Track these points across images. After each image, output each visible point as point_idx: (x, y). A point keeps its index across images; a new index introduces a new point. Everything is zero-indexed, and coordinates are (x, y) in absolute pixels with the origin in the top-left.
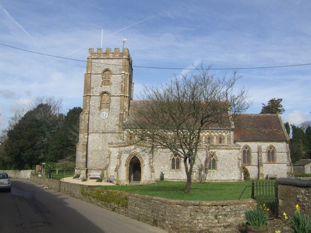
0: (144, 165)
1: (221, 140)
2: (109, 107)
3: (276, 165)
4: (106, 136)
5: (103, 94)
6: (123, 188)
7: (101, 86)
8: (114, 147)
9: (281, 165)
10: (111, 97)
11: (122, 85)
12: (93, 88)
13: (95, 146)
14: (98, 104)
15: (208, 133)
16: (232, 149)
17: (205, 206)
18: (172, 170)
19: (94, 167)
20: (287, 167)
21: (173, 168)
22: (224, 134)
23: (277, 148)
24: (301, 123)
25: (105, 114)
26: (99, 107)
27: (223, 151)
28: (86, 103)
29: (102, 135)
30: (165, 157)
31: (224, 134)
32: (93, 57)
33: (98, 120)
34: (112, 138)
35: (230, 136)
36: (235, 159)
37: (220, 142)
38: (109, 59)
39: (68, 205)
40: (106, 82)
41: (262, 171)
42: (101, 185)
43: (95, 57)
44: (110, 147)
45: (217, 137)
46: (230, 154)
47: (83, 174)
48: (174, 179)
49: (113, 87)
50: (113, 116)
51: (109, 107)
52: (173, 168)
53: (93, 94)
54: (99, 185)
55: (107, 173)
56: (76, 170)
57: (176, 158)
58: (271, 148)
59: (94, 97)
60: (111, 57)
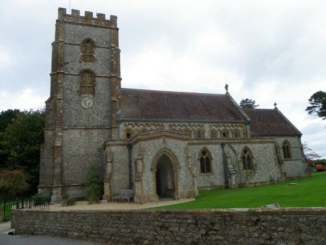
0: (180, 168)
1: (236, 134)
2: (93, 93)
3: (293, 162)
5: (84, 72)
6: (15, 211)
7: (80, 62)
8: (118, 145)
9: (297, 161)
10: (97, 79)
11: (112, 62)
12: (68, 63)
14: (76, 87)
15: (223, 128)
16: (266, 142)
17: (265, 221)
19: (73, 182)
20: (303, 163)
21: (203, 171)
22: (240, 128)
23: (291, 143)
25: (88, 101)
26: (78, 91)
27: (257, 145)
28: (57, 84)
29: (83, 132)
31: (240, 128)
32: (66, 20)
33: (76, 110)
35: (246, 131)
36: (271, 155)
37: (236, 136)
38: (90, 25)
40: (88, 57)
42: (164, 205)
45: (221, 132)
46: (265, 148)
47: (57, 194)
48: (206, 187)
50: (101, 105)
51: (93, 93)
54: (170, 204)
55: (110, 186)
56: (39, 190)
58: (285, 143)
59: (70, 77)
60: (93, 24)
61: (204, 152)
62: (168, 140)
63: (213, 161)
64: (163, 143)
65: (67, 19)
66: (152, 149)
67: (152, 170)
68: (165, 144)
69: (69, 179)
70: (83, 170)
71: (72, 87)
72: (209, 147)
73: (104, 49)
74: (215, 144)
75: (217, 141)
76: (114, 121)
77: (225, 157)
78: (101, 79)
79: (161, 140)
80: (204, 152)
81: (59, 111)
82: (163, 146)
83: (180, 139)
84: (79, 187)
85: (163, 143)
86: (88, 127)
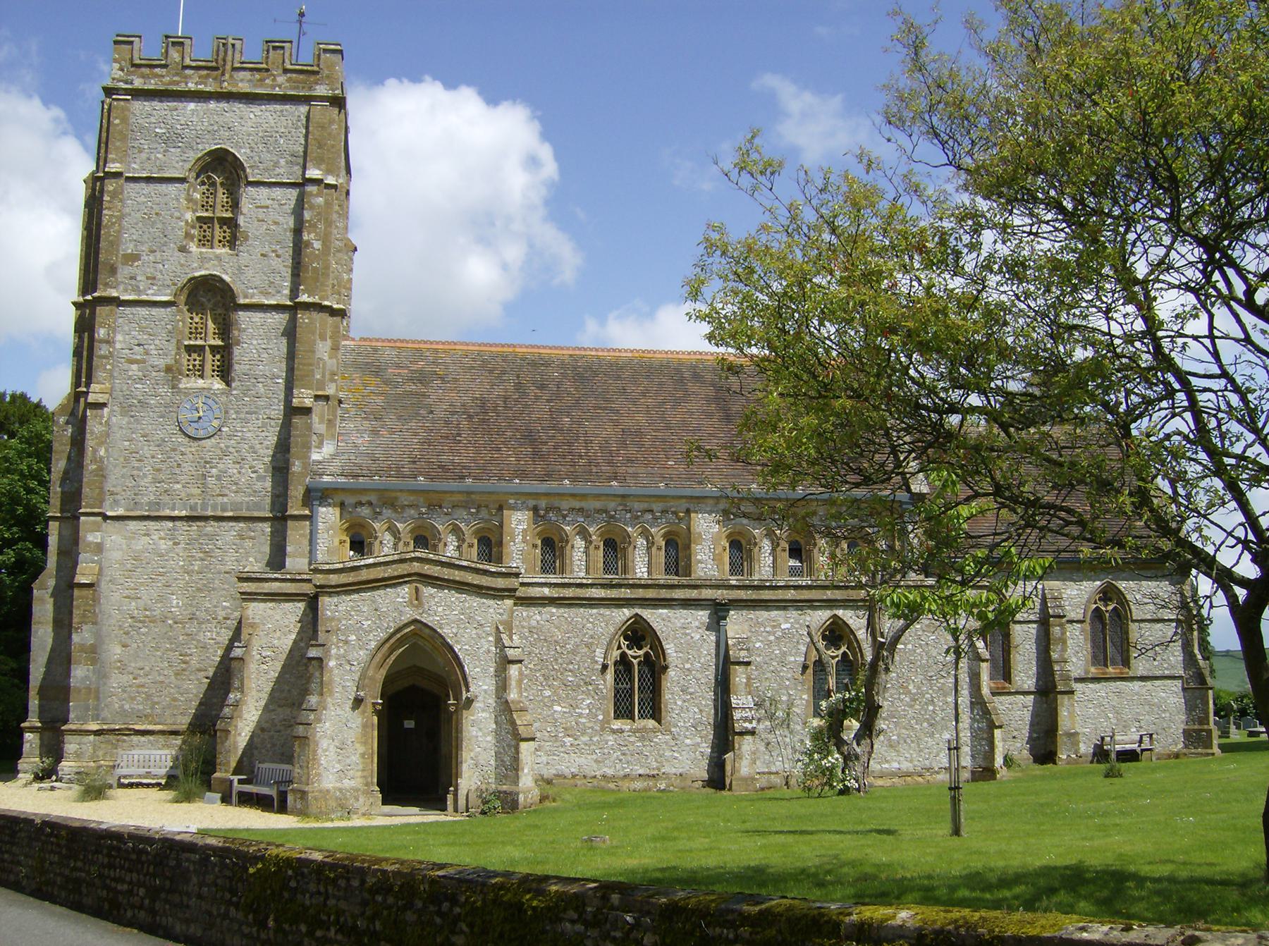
4: (212, 537)
7: (183, 249)
9: (1158, 683)
12: (135, 257)
13: (143, 592)
18: (617, 724)
21: (623, 710)
24: (423, 85)
30: (574, 652)
32: (138, 83)
34: (248, 543)
39: (771, 870)
41: (1072, 714)
43: (152, 85)
44: (249, 597)
47: (78, 756)
49: (250, 253)
51: (225, 372)
52: (623, 710)
53: (137, 290)
57: (636, 655)
59: (143, 311)
60: (244, 87)
61: (638, 633)
62: (428, 591)
63: (671, 673)
64: (410, 603)
65: (143, 76)
66: (366, 623)
67: (358, 702)
68: (420, 605)
69: (127, 707)
70: (176, 674)
71: (147, 353)
72: (656, 618)
73: (278, 192)
74: (687, 604)
75: (694, 594)
76: (297, 492)
77: (725, 667)
78: (257, 317)
79: (405, 591)
80: (638, 633)
81: (95, 451)
82: (409, 614)
83: (479, 590)
84: (161, 739)
85: (410, 603)
86: (199, 512)
